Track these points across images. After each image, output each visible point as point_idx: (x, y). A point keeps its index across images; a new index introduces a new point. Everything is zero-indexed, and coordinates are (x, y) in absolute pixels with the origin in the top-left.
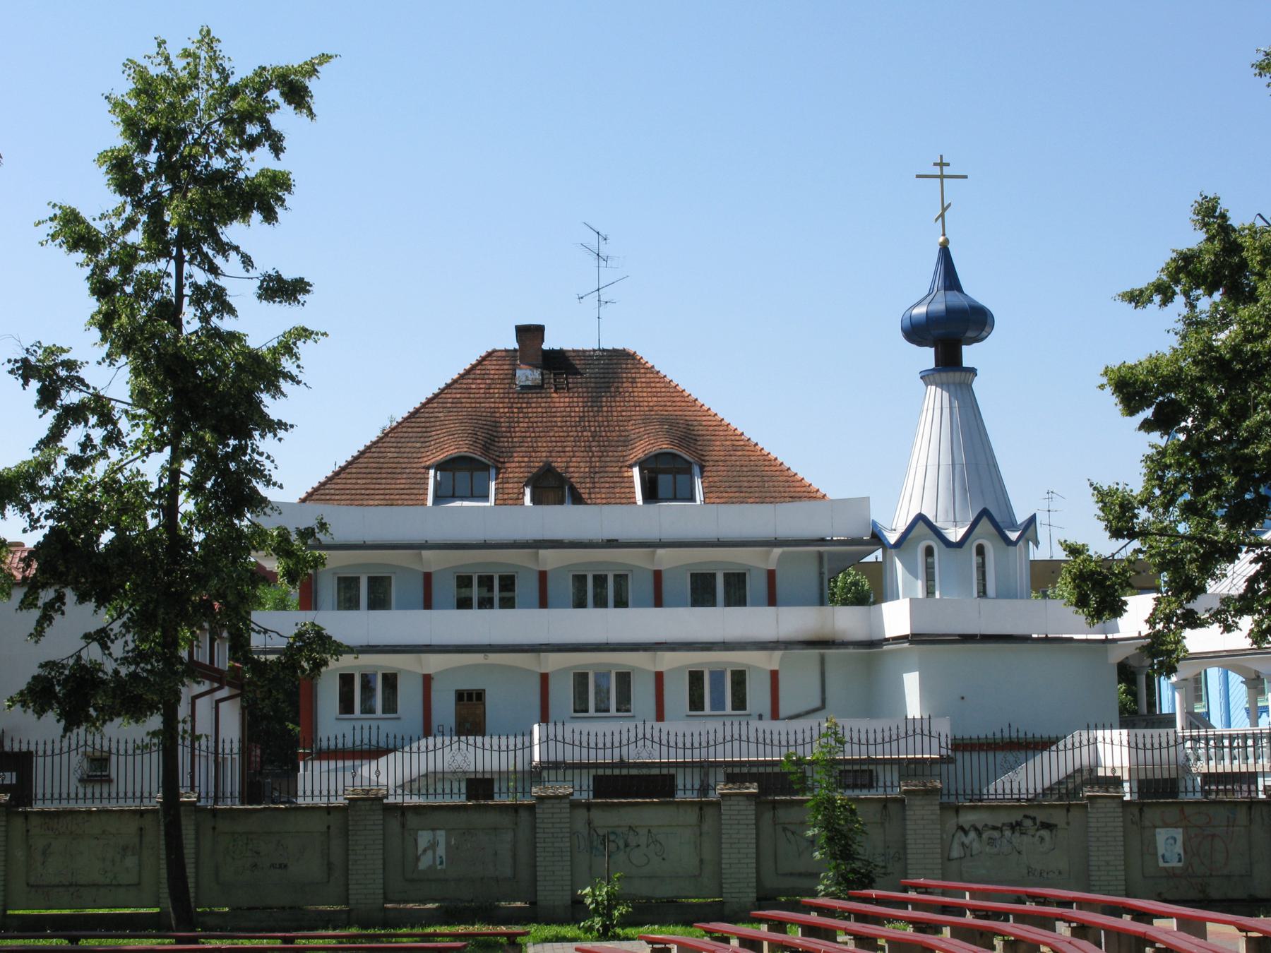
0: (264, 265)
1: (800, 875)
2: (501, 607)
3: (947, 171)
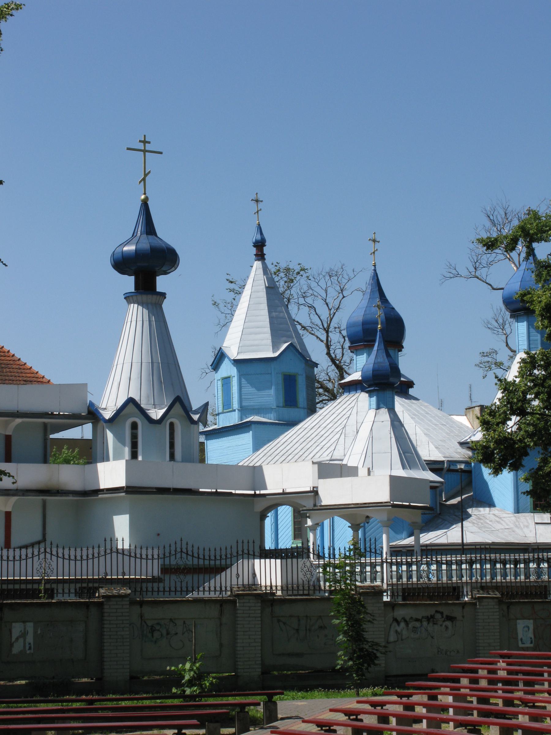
1: (291, 655)
2: (114, 460)
3: (148, 147)
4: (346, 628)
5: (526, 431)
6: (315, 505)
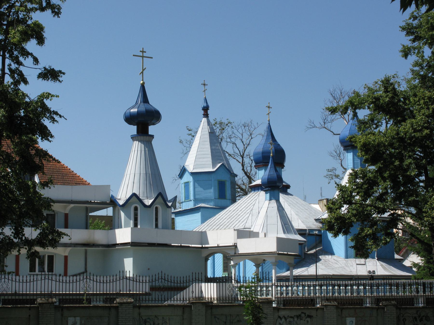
0: (44, 63)
3: (145, 54)
6: (235, 253)
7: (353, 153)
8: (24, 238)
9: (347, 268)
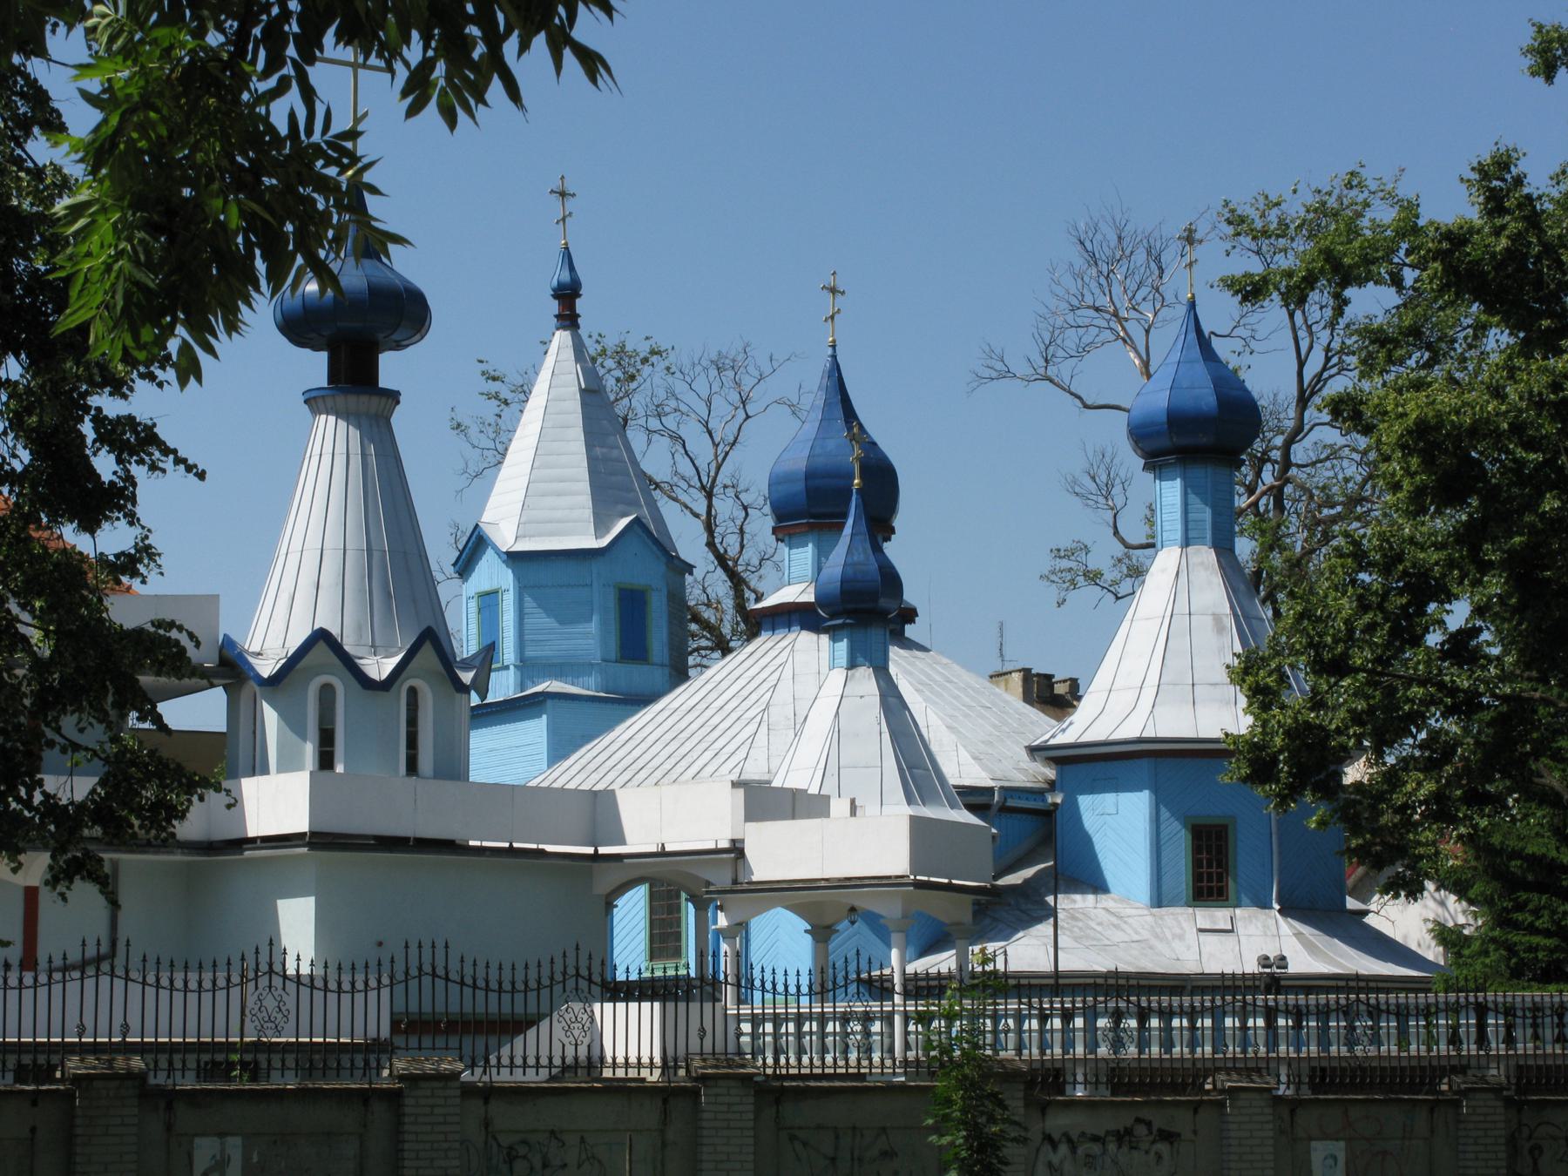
2: (279, 771)
4: (964, 1154)
5: (1351, 711)
6: (735, 882)
7: (1184, 479)
8: (38, 798)
9: (1159, 946)
